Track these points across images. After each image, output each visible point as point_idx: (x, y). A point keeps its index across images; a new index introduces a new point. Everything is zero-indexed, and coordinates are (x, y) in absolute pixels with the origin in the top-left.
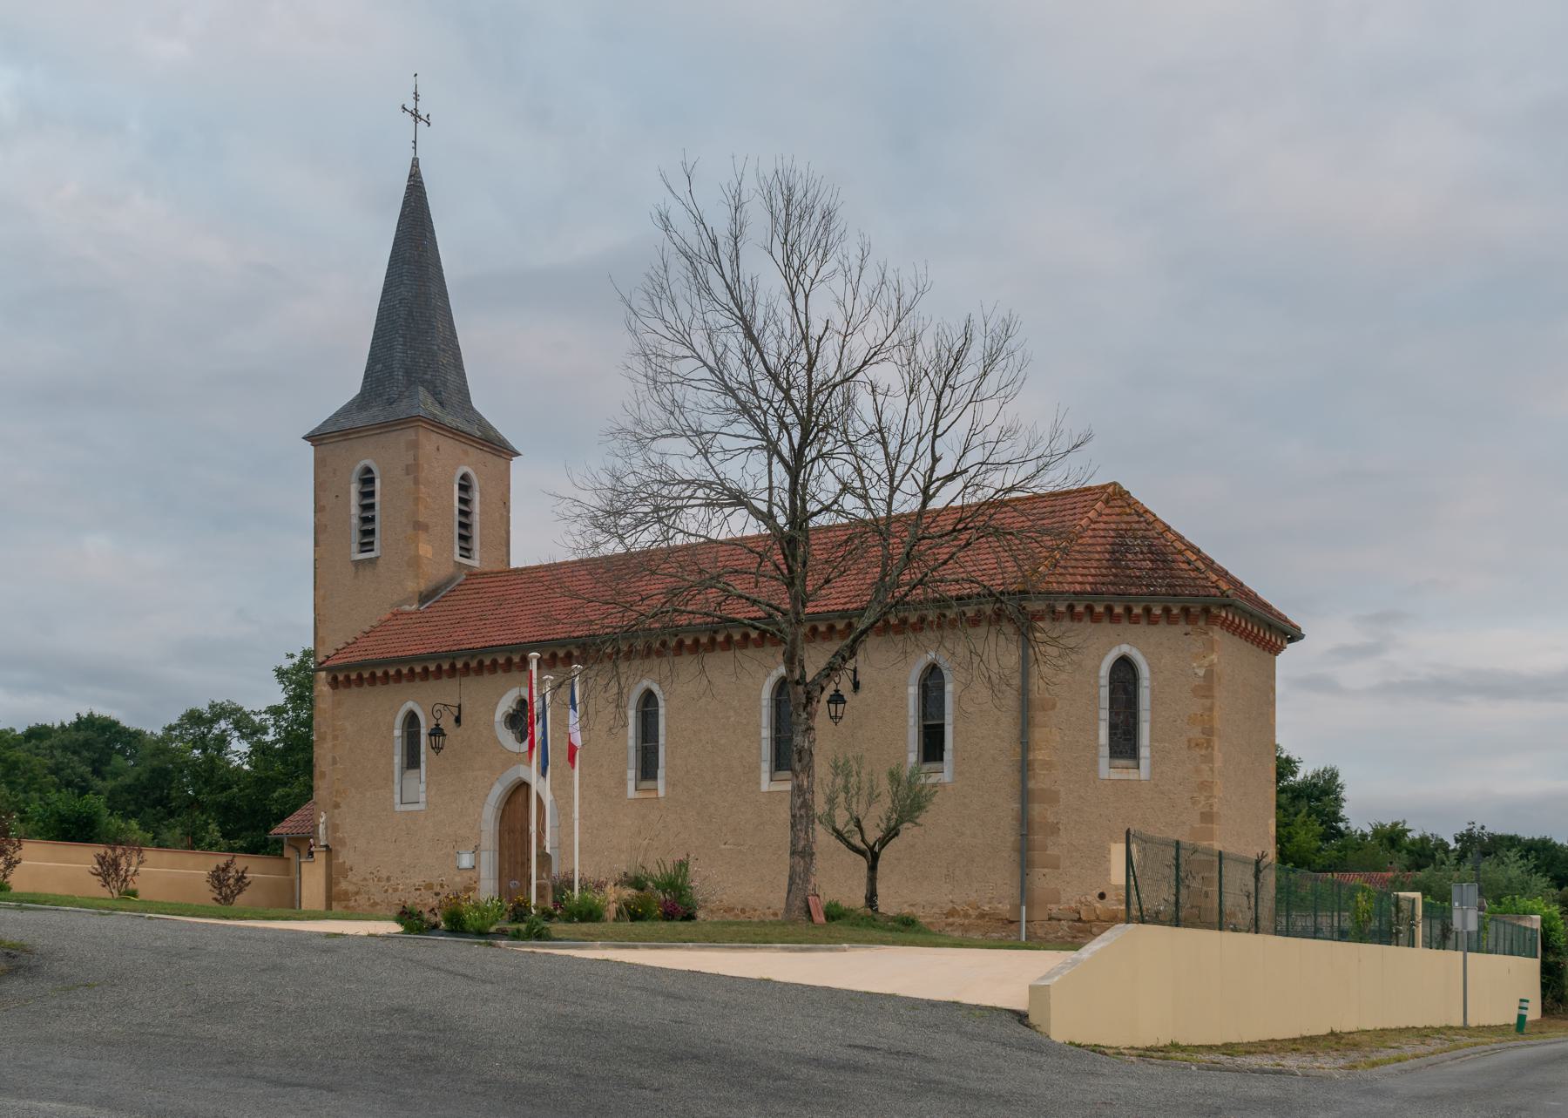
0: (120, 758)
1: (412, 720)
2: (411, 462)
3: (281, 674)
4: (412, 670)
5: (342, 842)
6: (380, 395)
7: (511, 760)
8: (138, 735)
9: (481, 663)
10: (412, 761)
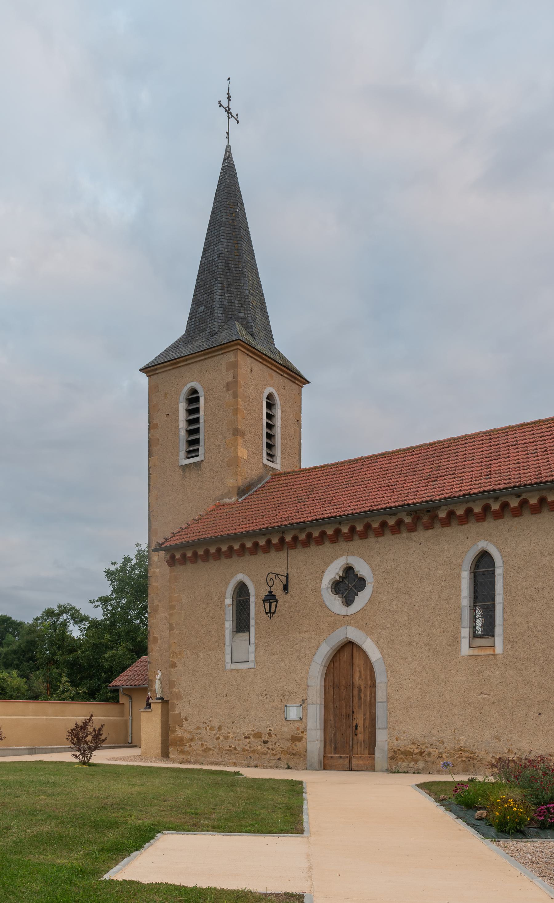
0: (11, 636)
1: (242, 591)
2: (231, 379)
3: (109, 574)
4: (243, 546)
5: (178, 696)
6: (203, 330)
7: (339, 621)
8: (20, 624)
9: (309, 536)
10: (242, 624)
